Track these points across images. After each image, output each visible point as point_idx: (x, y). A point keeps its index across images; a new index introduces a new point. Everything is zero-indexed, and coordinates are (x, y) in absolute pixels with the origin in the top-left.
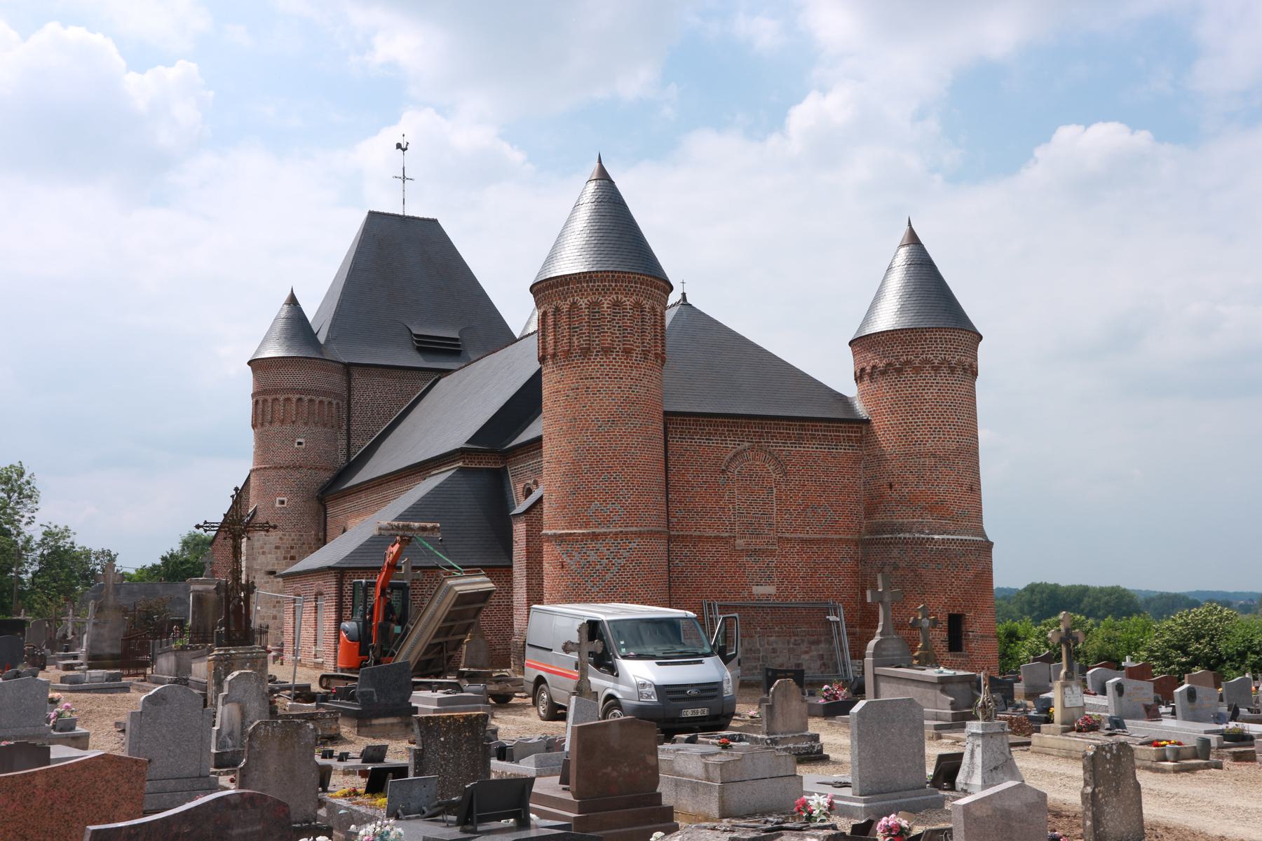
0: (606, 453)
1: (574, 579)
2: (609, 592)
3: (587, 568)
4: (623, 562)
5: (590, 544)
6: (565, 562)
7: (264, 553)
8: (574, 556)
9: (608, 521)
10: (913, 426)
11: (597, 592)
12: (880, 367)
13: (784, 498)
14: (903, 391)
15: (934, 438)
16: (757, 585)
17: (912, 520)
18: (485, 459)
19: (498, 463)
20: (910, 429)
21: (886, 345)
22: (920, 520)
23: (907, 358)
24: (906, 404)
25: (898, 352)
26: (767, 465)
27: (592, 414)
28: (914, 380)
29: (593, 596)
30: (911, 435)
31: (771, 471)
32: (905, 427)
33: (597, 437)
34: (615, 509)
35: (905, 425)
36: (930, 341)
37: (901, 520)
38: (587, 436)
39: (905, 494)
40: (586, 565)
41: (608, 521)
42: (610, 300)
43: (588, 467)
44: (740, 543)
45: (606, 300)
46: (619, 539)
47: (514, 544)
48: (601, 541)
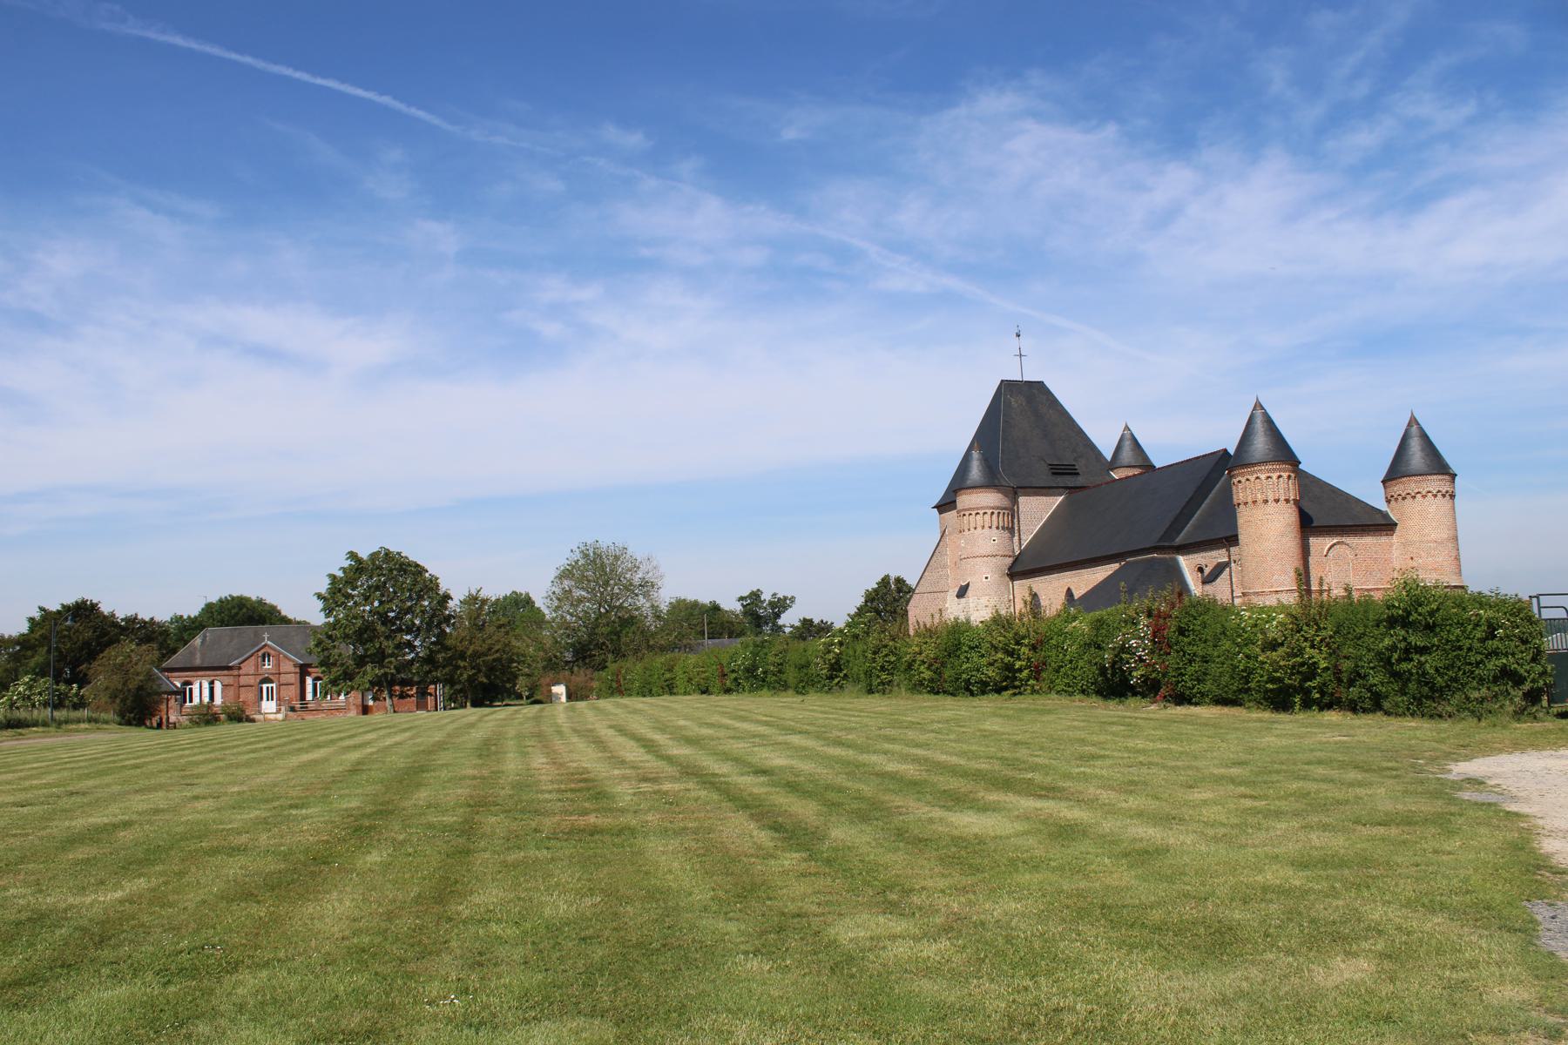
7: (977, 610)
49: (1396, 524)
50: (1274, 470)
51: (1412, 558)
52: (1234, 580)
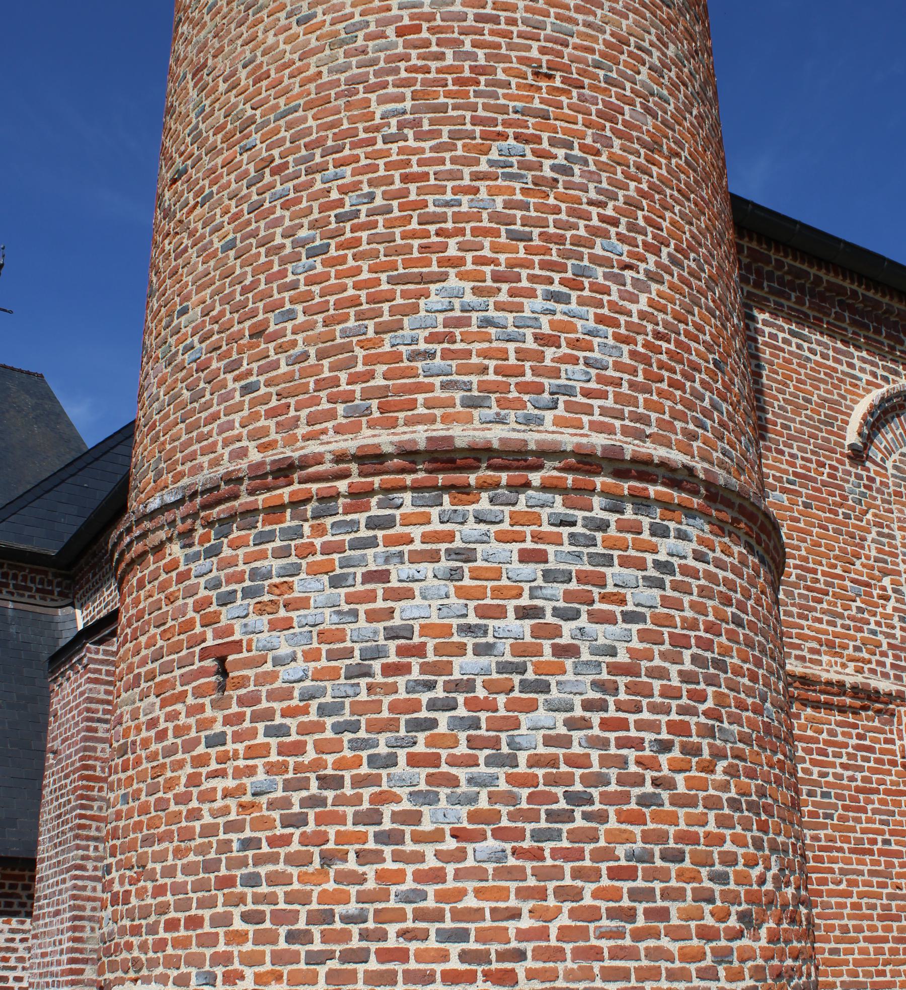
1: (298, 749)
2: (538, 836)
3: (389, 670)
5: (407, 521)
6: (237, 646)
8: (302, 604)
9: (524, 388)
18: (15, 577)
19: (51, 592)
29: (431, 862)
40: (378, 653)
41: (524, 388)
43: (408, 104)
46: (597, 501)
47: (51, 759)
48: (484, 503)
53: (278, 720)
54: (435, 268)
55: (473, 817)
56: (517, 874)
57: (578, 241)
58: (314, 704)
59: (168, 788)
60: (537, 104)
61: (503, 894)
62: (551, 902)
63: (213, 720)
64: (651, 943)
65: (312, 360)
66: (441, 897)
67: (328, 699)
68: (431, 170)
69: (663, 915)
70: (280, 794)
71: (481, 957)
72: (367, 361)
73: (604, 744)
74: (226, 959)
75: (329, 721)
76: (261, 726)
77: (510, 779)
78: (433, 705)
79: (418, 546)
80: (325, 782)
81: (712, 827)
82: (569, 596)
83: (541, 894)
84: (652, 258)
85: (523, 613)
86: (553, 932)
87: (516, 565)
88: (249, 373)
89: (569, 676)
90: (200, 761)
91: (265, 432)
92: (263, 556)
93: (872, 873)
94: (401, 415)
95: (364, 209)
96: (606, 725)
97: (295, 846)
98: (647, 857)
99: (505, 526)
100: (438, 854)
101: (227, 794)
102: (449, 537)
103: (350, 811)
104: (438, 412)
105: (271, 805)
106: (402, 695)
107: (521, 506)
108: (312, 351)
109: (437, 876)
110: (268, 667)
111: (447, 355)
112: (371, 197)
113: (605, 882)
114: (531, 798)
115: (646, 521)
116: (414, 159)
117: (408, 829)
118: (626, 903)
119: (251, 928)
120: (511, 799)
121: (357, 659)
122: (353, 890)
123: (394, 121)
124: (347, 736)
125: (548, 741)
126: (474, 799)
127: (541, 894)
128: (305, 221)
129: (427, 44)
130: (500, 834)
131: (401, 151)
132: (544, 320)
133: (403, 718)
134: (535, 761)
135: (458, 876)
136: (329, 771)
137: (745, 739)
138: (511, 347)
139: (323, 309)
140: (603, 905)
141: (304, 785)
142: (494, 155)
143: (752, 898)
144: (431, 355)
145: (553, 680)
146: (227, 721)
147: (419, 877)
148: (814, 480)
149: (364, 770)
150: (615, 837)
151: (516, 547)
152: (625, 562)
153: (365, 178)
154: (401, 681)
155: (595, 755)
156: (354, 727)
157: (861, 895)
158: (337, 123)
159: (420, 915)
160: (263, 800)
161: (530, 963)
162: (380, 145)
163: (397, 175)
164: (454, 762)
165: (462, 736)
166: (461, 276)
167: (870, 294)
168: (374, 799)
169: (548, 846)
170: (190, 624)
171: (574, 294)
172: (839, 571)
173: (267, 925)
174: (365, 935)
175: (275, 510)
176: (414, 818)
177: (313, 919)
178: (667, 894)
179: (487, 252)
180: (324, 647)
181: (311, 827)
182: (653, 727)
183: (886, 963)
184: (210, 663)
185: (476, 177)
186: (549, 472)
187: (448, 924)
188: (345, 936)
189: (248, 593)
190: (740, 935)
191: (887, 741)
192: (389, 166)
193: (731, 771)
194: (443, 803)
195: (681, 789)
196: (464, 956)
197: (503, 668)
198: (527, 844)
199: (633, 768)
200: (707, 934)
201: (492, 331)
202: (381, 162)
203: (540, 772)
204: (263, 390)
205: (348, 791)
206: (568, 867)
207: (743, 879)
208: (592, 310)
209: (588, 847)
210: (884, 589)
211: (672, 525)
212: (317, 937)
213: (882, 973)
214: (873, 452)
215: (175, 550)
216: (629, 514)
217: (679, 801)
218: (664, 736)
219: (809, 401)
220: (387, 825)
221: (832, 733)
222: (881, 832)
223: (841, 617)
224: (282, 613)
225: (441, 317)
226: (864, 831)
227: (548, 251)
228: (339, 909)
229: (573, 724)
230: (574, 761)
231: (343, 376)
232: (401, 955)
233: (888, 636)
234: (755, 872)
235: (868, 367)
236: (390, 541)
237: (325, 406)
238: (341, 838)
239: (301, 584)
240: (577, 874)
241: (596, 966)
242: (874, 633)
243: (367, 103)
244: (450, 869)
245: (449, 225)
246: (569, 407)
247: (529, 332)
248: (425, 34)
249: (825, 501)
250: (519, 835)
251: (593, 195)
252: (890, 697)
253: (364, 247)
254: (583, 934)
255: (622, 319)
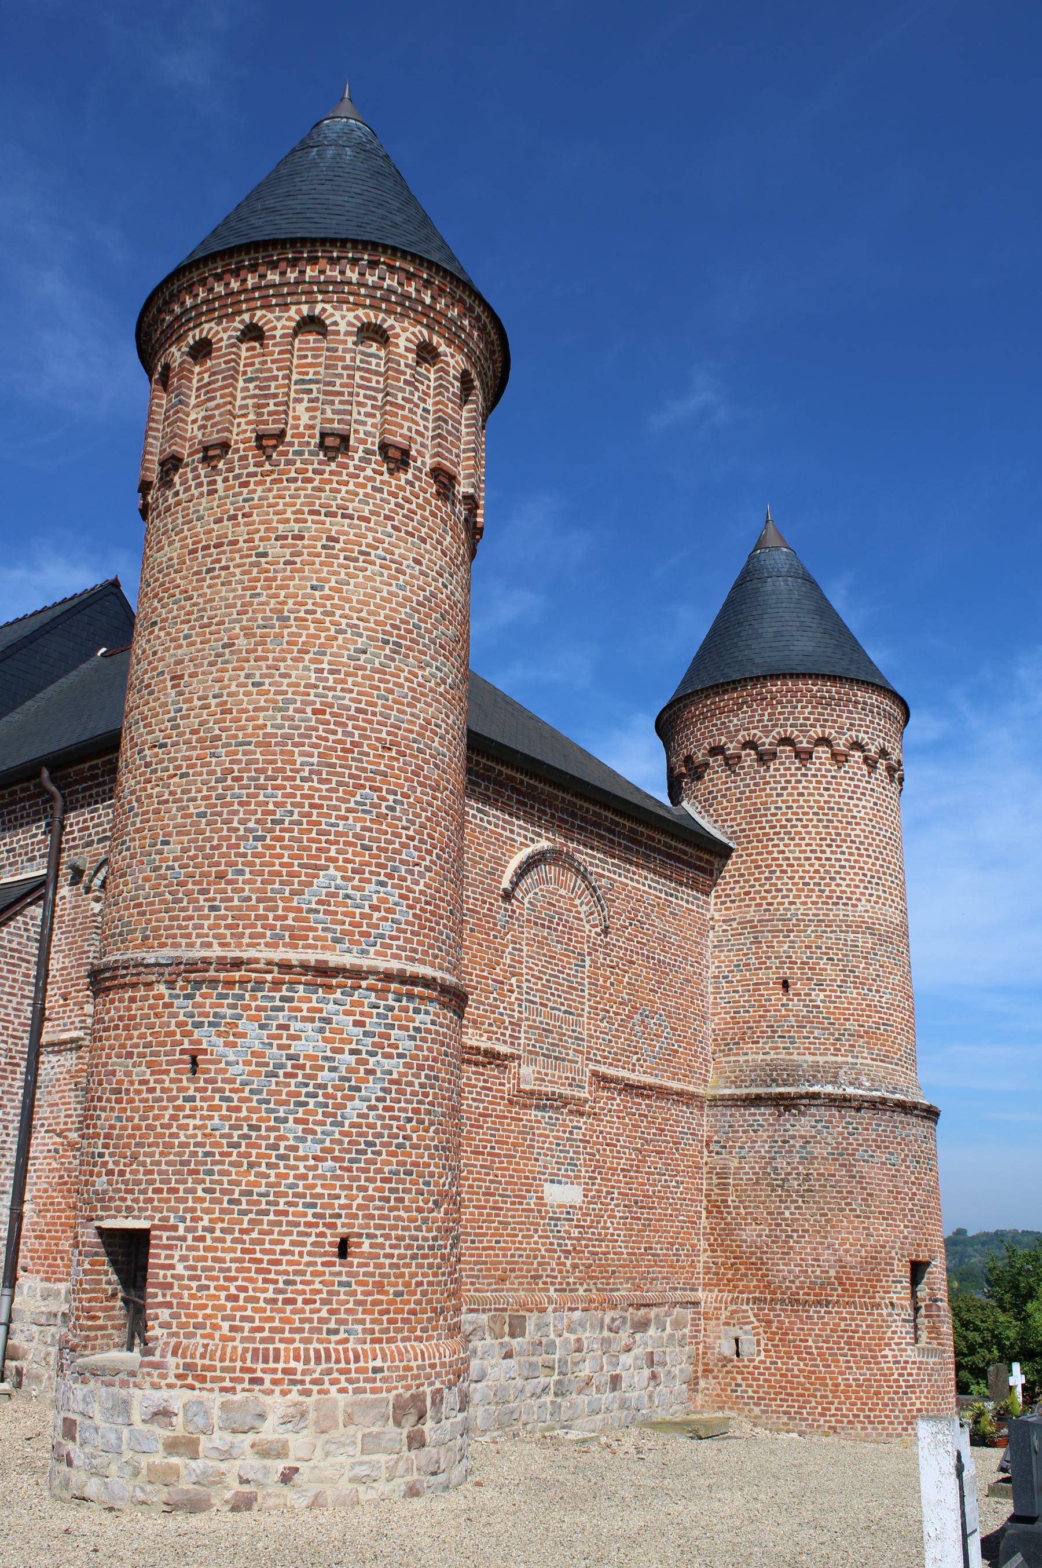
0: (373, 730)
2: (351, 1161)
4: (396, 1066)
5: (301, 1000)
6: (204, 1052)
8: (243, 1035)
9: (362, 934)
10: (833, 866)
11: (315, 1158)
12: (763, 744)
13: (601, 982)
14: (813, 795)
15: (871, 895)
16: (553, 1181)
17: (834, 1058)
20: (827, 872)
21: (780, 702)
22: (849, 1059)
23: (823, 732)
24: (819, 821)
25: (805, 719)
26: (577, 902)
27: (338, 613)
28: (833, 777)
29: (302, 1170)
30: (828, 885)
31: (582, 916)
32: (816, 867)
33: (350, 680)
34: (385, 901)
35: (817, 863)
36: (863, 709)
37: (810, 1058)
38: (321, 671)
39: (818, 1003)
40: (282, 1066)
41: (362, 934)
42: (413, 333)
43: (315, 760)
44: (527, 1073)
45: (404, 330)
46: (391, 996)
48: (338, 994)
49: (724, 852)
50: (407, 307)
51: (785, 985)
52: (54, 965)
53: (227, 1094)
54: (323, 862)
55: (323, 1150)
56: (340, 1178)
57: (395, 851)
58: (247, 1088)
59: (156, 1118)
60: (382, 768)
61: (333, 1187)
62: (355, 1192)
63: (188, 1088)
64: (396, 1213)
65: (253, 902)
66: (306, 1187)
67: (255, 1086)
68: (325, 803)
69: (401, 1200)
70: (227, 1131)
71: (322, 1216)
72: (284, 909)
73: (383, 1118)
74: (193, 1210)
75: (255, 1098)
76: (217, 1096)
77: (341, 1133)
78: (308, 1095)
79: (305, 1013)
80: (251, 1127)
81: (426, 1159)
82: (374, 1044)
83: (350, 1188)
84: (428, 858)
85: (353, 1052)
86: (354, 1206)
87: (351, 1027)
88: (214, 899)
89: (371, 1084)
90: (181, 1108)
91: (224, 936)
92: (221, 1006)
93: (482, 1167)
94: (301, 943)
95: (287, 819)
96: (385, 1109)
97: (234, 1158)
98: (397, 1173)
99: (347, 1007)
100: (305, 1167)
101: (195, 1127)
102: (321, 1011)
103: (264, 1143)
104: (319, 943)
105: (222, 1136)
106: (293, 1088)
107: (355, 998)
108: (254, 897)
109: (304, 1177)
110: (223, 1065)
111: (326, 912)
112: (292, 813)
113: (379, 1184)
114: (349, 1143)
115: (411, 1006)
116: (317, 794)
117: (292, 1154)
118: (387, 1194)
119: (208, 1196)
120: (340, 1142)
121: (271, 1068)
122: (264, 1181)
123: (307, 768)
124: (264, 1106)
125: (359, 1116)
126: (323, 1142)
127: (350, 1188)
128: (253, 818)
129: (328, 723)
130: (334, 1159)
131: (310, 788)
132: (375, 896)
133: (293, 1100)
134: (353, 1125)
135: (314, 1177)
136: (254, 1122)
137: (443, 1115)
138: (358, 911)
139: (261, 873)
140: (377, 1194)
141: (240, 1127)
142: (358, 798)
143: (440, 1193)
144: (317, 911)
145: (363, 1086)
146: (196, 1090)
147: (296, 1177)
148: (478, 913)
149: (272, 1123)
150: (385, 1163)
151: (352, 1018)
152: (401, 1027)
153: (289, 800)
154: (293, 1081)
155: (379, 1123)
156: (268, 1102)
157: (474, 1180)
158: (274, 762)
159: (295, 1195)
160: (218, 1133)
161: (343, 1220)
162: (298, 782)
163: (307, 802)
164: (315, 1123)
165: (320, 1111)
166: (337, 868)
167: (532, 782)
168: (277, 1138)
169: (355, 1166)
170: (173, 1034)
171: (390, 882)
172: (485, 974)
173: (217, 1195)
174: (268, 1203)
175: (229, 984)
176: (295, 1149)
177: (242, 1193)
178: (405, 1191)
179: (349, 856)
180: (254, 1060)
181: (243, 1149)
182: (405, 1110)
183: (484, 1221)
184: (186, 1057)
185: (348, 810)
186: (371, 981)
187: (308, 1200)
188: (259, 1203)
189: (211, 1024)
190: (432, 1211)
191: (501, 1084)
192: (303, 796)
193: (436, 1132)
194: (309, 1143)
195: (415, 1141)
196: (314, 1215)
197: (341, 1079)
198: (346, 1164)
199: (395, 1130)
200: (420, 1210)
201: (349, 901)
202: (298, 793)
203: (354, 1130)
204: (223, 912)
205: (263, 1133)
206: (363, 1176)
207: (436, 1184)
208: (398, 891)
209: (373, 1167)
210: (511, 985)
211: (423, 1007)
212: (244, 1202)
213: (481, 1228)
214: (518, 894)
215: (162, 988)
216: (404, 1003)
217: (415, 1147)
218: (410, 1115)
219: (482, 858)
220: (282, 1151)
221: (469, 1078)
222: (490, 1141)
223: (483, 1004)
224: (231, 1038)
225: (324, 891)
226: (480, 1140)
227: (379, 857)
228: (256, 1190)
229: (371, 1108)
230: (370, 1126)
231: (271, 915)
232: (285, 1213)
233: (510, 1016)
234: (442, 1181)
235: (522, 832)
236: (291, 1009)
237: (260, 930)
238: (258, 1155)
239: (243, 1025)
240: (367, 1179)
241: (372, 1223)
242: (501, 1014)
243: (292, 753)
244: (311, 1174)
245: (332, 838)
246: (383, 945)
247: (367, 903)
248: (328, 717)
249: (483, 927)
250: (342, 1160)
251: (404, 823)
252: (506, 1057)
253: (286, 843)
254: (367, 1207)
255: (411, 895)
